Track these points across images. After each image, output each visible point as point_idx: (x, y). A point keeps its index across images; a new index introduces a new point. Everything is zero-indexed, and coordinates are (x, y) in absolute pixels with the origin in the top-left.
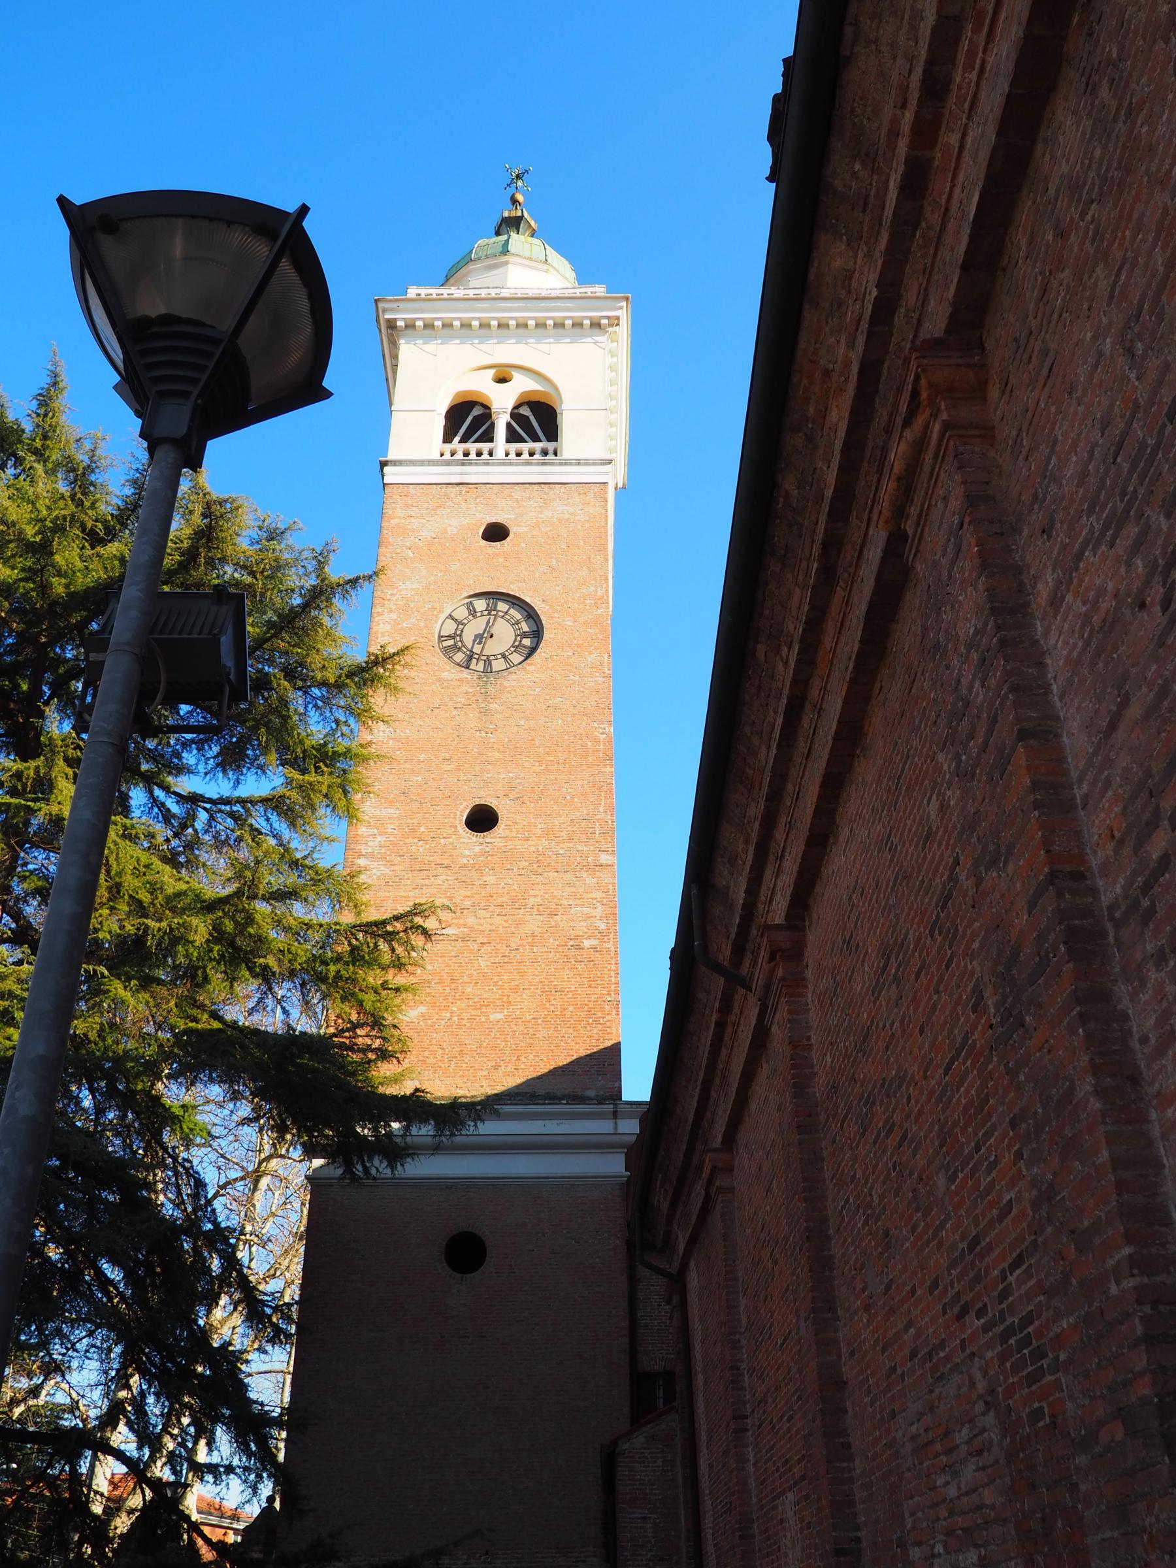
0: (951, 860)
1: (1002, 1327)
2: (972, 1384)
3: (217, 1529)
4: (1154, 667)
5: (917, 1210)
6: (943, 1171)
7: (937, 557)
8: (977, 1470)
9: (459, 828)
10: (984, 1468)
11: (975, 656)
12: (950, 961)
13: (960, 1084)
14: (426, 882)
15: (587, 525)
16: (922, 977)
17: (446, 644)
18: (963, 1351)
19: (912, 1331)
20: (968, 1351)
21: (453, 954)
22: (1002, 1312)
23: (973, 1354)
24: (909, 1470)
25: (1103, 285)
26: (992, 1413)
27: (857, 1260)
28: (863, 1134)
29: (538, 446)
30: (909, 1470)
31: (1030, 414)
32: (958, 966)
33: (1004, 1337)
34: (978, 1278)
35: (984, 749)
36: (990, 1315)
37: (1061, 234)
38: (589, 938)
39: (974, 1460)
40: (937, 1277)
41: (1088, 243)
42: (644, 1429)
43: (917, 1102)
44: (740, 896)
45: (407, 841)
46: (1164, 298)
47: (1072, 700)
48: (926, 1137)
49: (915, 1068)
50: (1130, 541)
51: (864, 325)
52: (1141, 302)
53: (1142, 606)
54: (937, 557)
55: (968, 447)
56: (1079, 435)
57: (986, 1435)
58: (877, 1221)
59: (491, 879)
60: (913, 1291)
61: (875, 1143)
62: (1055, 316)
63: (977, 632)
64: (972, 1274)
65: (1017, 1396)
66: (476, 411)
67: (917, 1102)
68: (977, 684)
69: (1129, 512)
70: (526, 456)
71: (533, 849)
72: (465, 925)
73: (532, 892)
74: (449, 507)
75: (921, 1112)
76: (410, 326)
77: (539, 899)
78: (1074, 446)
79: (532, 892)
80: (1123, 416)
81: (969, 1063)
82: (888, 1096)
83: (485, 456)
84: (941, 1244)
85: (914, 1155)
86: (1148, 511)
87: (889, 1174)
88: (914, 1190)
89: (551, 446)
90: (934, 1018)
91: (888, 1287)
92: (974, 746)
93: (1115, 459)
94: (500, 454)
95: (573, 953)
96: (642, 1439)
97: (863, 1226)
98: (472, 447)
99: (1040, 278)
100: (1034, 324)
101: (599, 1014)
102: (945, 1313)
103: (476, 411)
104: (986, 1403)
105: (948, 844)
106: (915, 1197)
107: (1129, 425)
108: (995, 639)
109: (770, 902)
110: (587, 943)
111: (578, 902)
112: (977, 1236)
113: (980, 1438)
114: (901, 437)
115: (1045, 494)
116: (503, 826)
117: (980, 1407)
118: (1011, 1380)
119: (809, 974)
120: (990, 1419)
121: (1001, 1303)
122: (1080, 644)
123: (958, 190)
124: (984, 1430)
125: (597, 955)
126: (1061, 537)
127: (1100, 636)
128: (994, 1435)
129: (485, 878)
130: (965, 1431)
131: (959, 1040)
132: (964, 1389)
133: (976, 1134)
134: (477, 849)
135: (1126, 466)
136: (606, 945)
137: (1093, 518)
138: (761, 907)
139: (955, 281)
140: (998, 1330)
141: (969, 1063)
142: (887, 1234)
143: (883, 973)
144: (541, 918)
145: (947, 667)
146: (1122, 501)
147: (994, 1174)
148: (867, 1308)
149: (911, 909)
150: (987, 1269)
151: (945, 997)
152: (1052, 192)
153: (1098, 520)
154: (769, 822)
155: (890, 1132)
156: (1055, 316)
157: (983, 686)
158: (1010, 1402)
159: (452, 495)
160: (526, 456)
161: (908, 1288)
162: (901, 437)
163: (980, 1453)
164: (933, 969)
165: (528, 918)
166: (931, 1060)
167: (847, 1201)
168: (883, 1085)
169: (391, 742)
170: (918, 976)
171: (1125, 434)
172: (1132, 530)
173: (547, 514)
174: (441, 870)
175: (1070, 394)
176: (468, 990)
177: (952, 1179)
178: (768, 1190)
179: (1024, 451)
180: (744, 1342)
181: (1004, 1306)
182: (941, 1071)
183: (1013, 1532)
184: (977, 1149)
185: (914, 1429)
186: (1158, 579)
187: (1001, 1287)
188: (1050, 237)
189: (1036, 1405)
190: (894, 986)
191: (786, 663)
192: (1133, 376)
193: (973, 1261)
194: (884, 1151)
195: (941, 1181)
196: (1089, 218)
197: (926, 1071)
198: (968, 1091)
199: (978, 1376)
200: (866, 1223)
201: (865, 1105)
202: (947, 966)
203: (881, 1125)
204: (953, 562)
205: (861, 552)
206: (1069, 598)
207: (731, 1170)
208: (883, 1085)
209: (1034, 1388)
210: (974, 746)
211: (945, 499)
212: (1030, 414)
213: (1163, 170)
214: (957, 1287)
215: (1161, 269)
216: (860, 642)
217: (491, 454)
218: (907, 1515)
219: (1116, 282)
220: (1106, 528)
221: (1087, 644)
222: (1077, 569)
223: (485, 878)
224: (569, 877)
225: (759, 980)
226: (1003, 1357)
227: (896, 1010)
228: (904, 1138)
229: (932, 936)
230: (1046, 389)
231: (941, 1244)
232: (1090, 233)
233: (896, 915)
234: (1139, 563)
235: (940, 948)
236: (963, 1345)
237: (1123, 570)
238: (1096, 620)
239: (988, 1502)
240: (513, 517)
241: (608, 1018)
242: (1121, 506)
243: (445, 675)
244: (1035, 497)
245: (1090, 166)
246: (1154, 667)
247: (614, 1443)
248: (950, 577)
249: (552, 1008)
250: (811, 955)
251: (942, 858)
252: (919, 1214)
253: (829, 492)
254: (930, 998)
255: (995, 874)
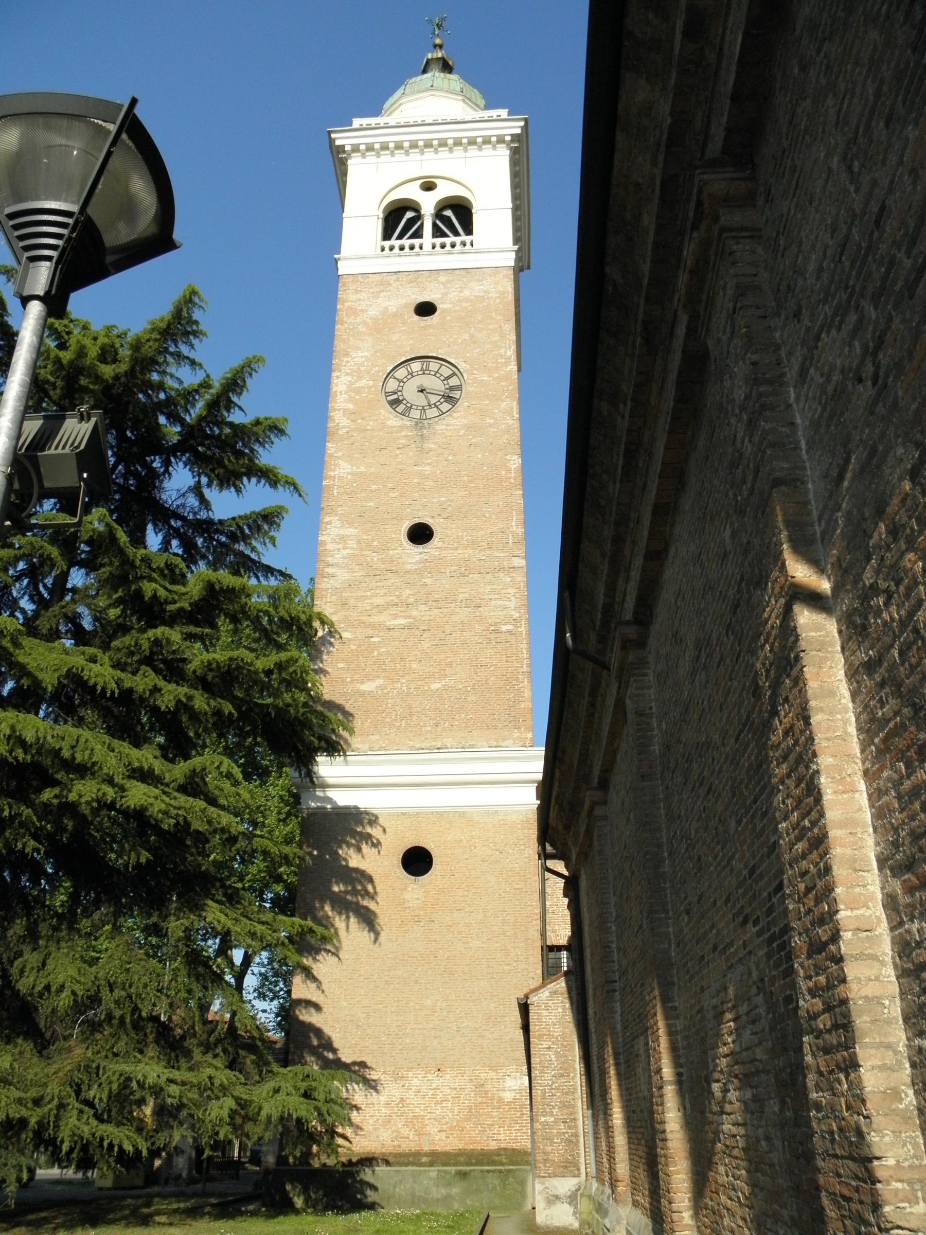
0: (739, 577)
1: (769, 934)
2: (750, 973)
3: (527, 1078)
4: (867, 431)
5: (718, 843)
6: (733, 817)
7: (720, 335)
8: (752, 1034)
9: (404, 542)
10: (756, 1033)
11: (745, 417)
12: (739, 655)
13: (745, 750)
14: (379, 584)
15: (498, 301)
16: (721, 667)
17: (390, 398)
18: (745, 949)
19: (714, 931)
20: (748, 949)
21: (402, 639)
22: (768, 923)
23: (750, 952)
24: (711, 1029)
25: (832, 112)
26: (761, 995)
27: (681, 877)
28: (685, 784)
29: (458, 240)
30: (711, 1029)
31: (784, 219)
32: (744, 659)
33: (772, 939)
34: (754, 897)
35: (751, 493)
36: (761, 925)
37: (804, 68)
38: (506, 624)
39: (750, 1026)
40: (729, 895)
41: (822, 76)
42: (549, 986)
43: (718, 763)
44: (601, 600)
45: (364, 553)
46: (873, 123)
47: (815, 454)
48: (723, 789)
49: (717, 736)
50: (851, 327)
51: (663, 148)
52: (857, 128)
53: (860, 380)
54: (720, 335)
55: (740, 246)
56: (817, 237)
57: (757, 1010)
58: (694, 849)
59: (429, 581)
60: (715, 903)
61: (693, 790)
62: (800, 138)
63: (745, 399)
64: (751, 893)
65: (777, 985)
66: (409, 215)
67: (718, 763)
68: (747, 440)
69: (850, 302)
70: (448, 248)
71: (461, 556)
72: (410, 617)
73: (461, 590)
74: (390, 291)
75: (720, 771)
76: (356, 149)
77: (467, 595)
78: (813, 247)
79: (461, 590)
80: (845, 223)
81: (750, 736)
82: (701, 757)
83: (417, 249)
84: (732, 870)
85: (716, 802)
86: (863, 303)
87: (701, 815)
88: (716, 829)
89: (468, 239)
90: (729, 699)
91: (701, 897)
92: (745, 489)
93: (840, 259)
94: (427, 247)
95: (493, 636)
96: (547, 994)
97: (685, 853)
98: (406, 242)
99: (789, 106)
100: (786, 143)
101: (514, 683)
102: (734, 920)
103: (409, 215)
104: (758, 988)
105: (737, 564)
106: (717, 834)
107: (850, 229)
108: (757, 405)
109: (623, 603)
110: (504, 628)
111: (496, 596)
112: (754, 866)
113: (754, 1012)
114: (691, 239)
115: (796, 285)
116: (437, 539)
117: (754, 990)
118: (773, 973)
119: (651, 658)
120: (760, 1000)
121: (768, 916)
122: (819, 409)
123: (728, 32)
124: (756, 1007)
125: (513, 637)
126: (806, 322)
127: (833, 403)
128: (762, 1011)
129: (424, 580)
130: (745, 1006)
131: (745, 717)
132: (745, 977)
133: (754, 790)
134: (418, 557)
135: (847, 264)
136: (519, 630)
137: (827, 308)
138: (616, 606)
139: (728, 108)
140: (766, 936)
141: (750, 736)
142: (699, 859)
143: (697, 661)
144: (469, 610)
145: (729, 424)
146: (845, 292)
147: (765, 821)
148: (688, 912)
149: (714, 613)
150: (760, 891)
151: (735, 683)
152: (798, 32)
153: (830, 308)
154: (618, 540)
155: (701, 784)
156: (800, 138)
157: (750, 441)
158: (773, 989)
159: (392, 282)
160: (448, 248)
161: (712, 900)
162: (691, 239)
163: (754, 1022)
164: (728, 661)
165: (458, 610)
166: (727, 731)
167: (675, 833)
168: (697, 747)
169: (349, 477)
170: (719, 665)
171: (847, 238)
172: (853, 318)
173: (467, 293)
174: (390, 575)
175: (811, 203)
176: (414, 666)
177: (739, 822)
178: (628, 820)
179: (782, 248)
180: (614, 928)
181: (770, 919)
182: (733, 740)
183: (773, 1080)
184: (755, 801)
185: (714, 1001)
186: (869, 359)
187: (768, 905)
188: (796, 71)
189: (788, 993)
190: (704, 672)
191: (623, 417)
192: (852, 189)
193: (751, 885)
194: (698, 798)
195: (733, 824)
196: (822, 54)
197: (724, 739)
198: (749, 758)
199: (753, 968)
200: (687, 849)
201: (687, 761)
202: (737, 660)
203: (696, 777)
204: (730, 339)
205: (673, 328)
206: (812, 371)
207: (605, 803)
208: (697, 747)
209: (787, 980)
210: (745, 489)
211: (724, 288)
212: (784, 219)
213: (876, 9)
214: (742, 903)
215: (871, 98)
216: (674, 401)
217: (421, 248)
218: (710, 1060)
219: (840, 110)
220: (835, 315)
221: (824, 409)
222: (817, 348)
223: (424, 580)
224: (489, 576)
225: (614, 664)
226: (769, 956)
227: (705, 691)
228: (710, 789)
229: (727, 635)
230: (795, 200)
231: (732, 870)
232: (824, 68)
233: (705, 618)
234: (857, 343)
235: (732, 646)
236: (745, 945)
237: (846, 350)
238: (830, 389)
239: (758, 1057)
240: (439, 296)
241: (521, 685)
242: (844, 297)
243: (390, 423)
244: (789, 286)
245: (824, 8)
246: (867, 431)
247: (527, 997)
248: (728, 352)
249: (478, 679)
250: (653, 643)
251: (733, 575)
252: (719, 847)
253: (645, 282)
254: (726, 684)
255: (759, 592)
